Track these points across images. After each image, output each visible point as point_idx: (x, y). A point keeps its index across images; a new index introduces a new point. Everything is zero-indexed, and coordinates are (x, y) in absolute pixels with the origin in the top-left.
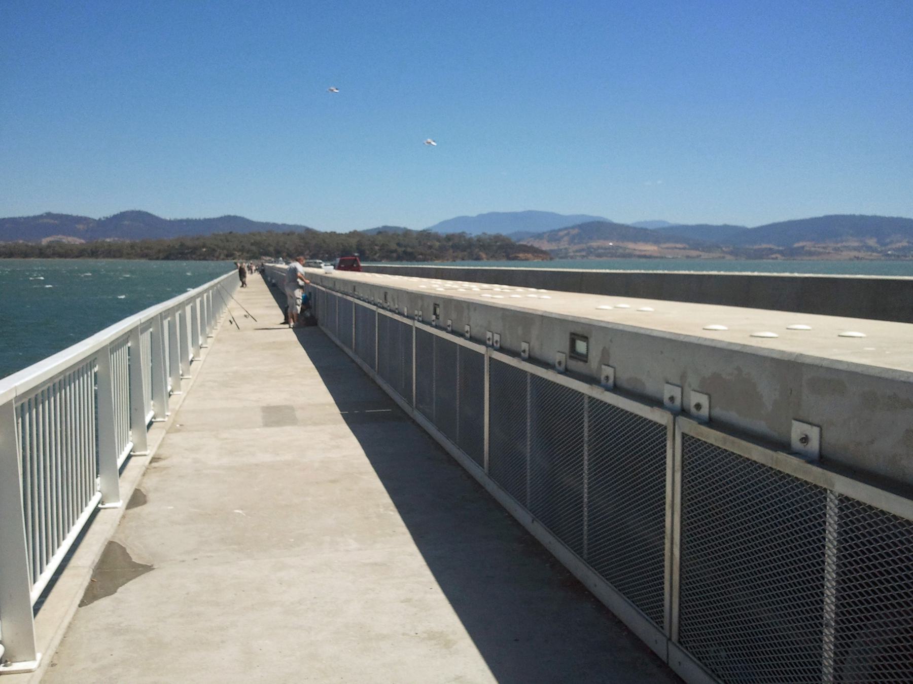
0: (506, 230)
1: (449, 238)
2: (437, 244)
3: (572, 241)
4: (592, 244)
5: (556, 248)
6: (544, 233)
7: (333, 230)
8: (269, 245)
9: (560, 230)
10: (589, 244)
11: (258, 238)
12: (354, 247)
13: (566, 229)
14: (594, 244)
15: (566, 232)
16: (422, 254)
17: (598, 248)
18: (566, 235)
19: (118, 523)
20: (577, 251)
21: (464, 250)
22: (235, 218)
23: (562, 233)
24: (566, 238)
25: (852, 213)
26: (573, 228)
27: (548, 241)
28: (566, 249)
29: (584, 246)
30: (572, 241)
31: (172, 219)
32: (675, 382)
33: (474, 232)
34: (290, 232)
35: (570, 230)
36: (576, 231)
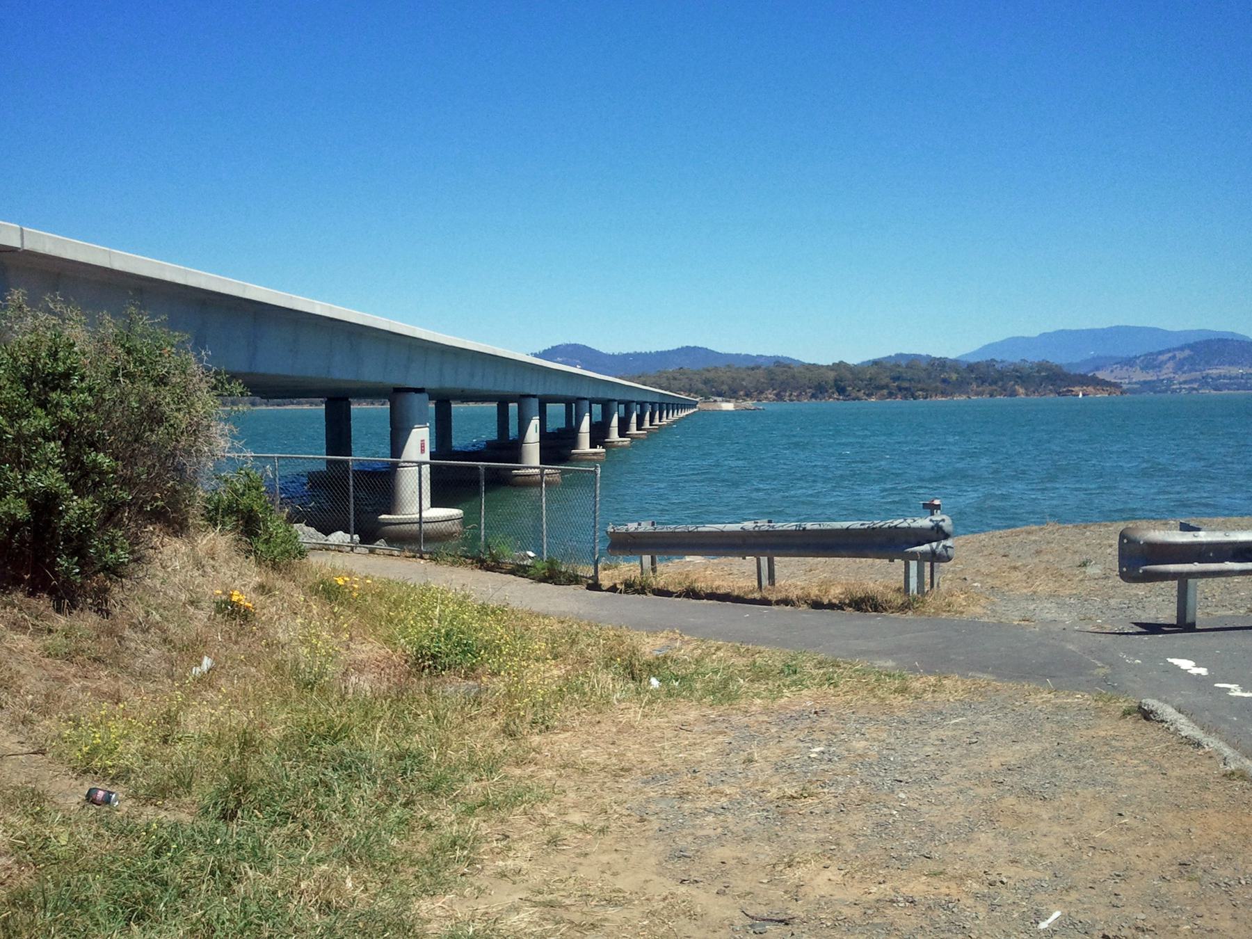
0: (1060, 358)
1: (971, 368)
2: (954, 376)
3: (1180, 366)
4: (1210, 372)
5: (1155, 378)
6: (1136, 357)
7: (899, 352)
8: (723, 383)
9: (1160, 353)
10: (1204, 373)
11: (711, 375)
12: (832, 383)
13: (1169, 351)
14: (1214, 372)
15: (1170, 355)
16: (922, 390)
17: (1220, 377)
18: (1170, 359)
19: (493, 604)
20: (1185, 382)
21: (994, 382)
22: (695, 349)
23: (1161, 358)
24: (1171, 365)
25: (888, 354)
26: (1182, 349)
27: (1142, 369)
28: (1168, 379)
29: (1197, 374)
30: (1180, 366)
31: (616, 353)
32: (593, 420)
33: (1012, 358)
34: (753, 364)
35: (1177, 353)
36: (1187, 353)
